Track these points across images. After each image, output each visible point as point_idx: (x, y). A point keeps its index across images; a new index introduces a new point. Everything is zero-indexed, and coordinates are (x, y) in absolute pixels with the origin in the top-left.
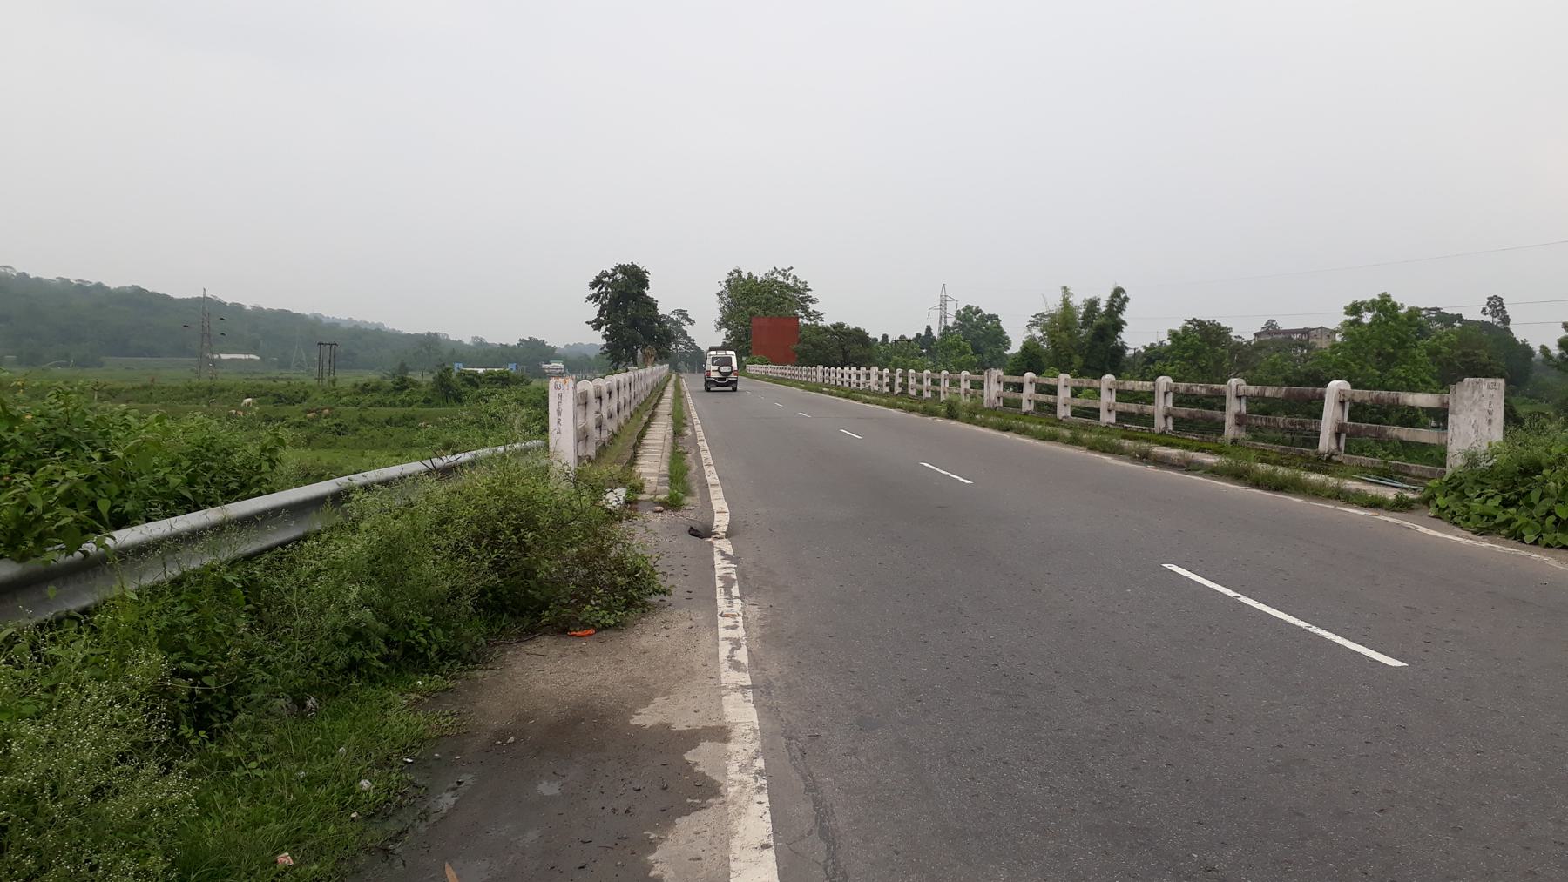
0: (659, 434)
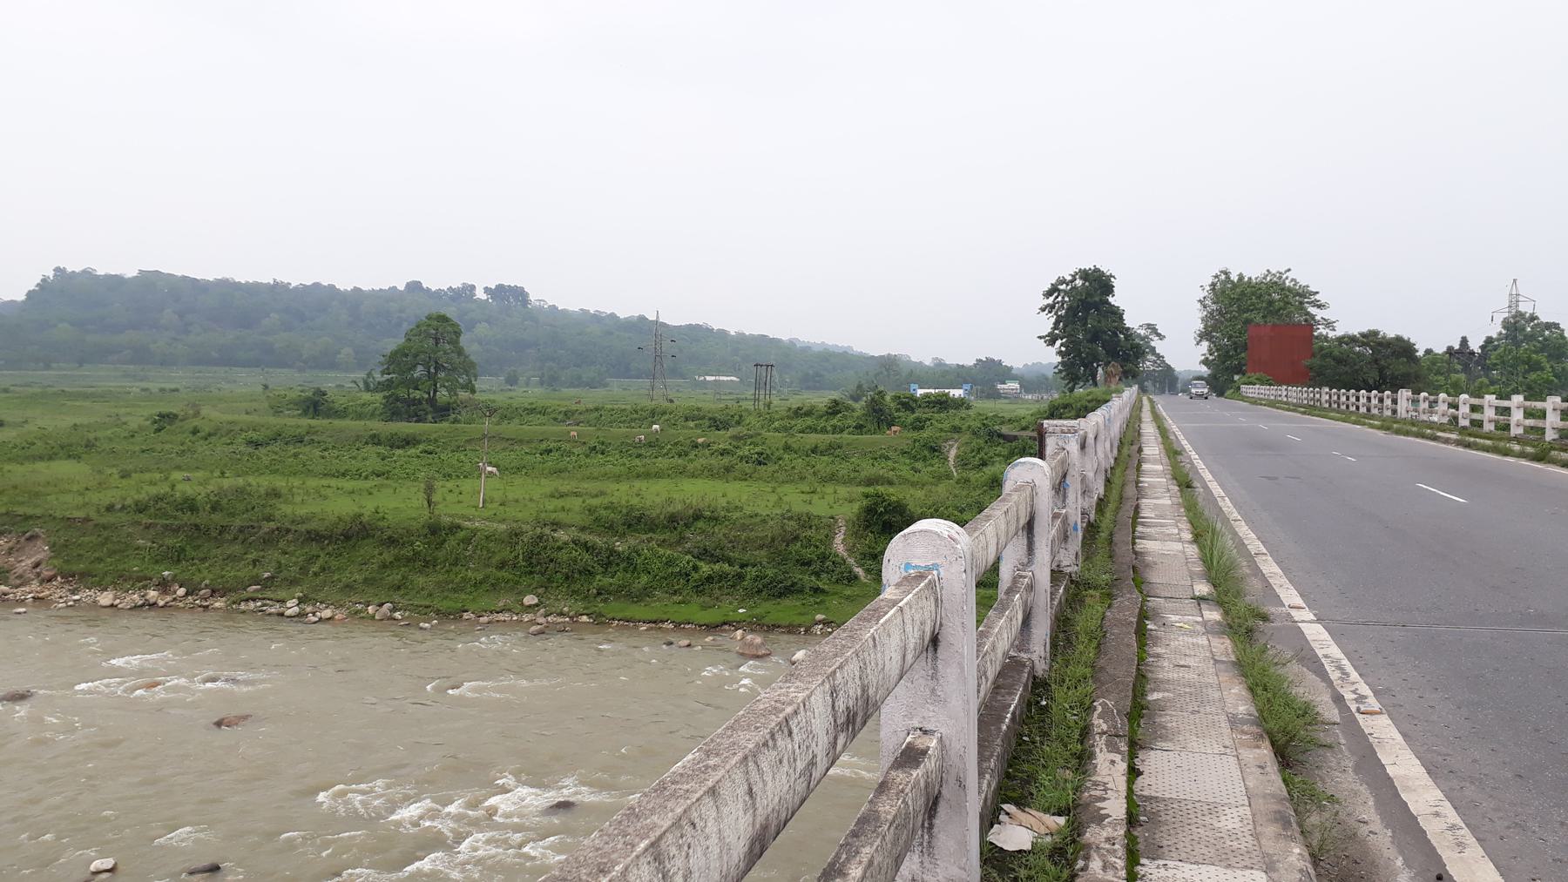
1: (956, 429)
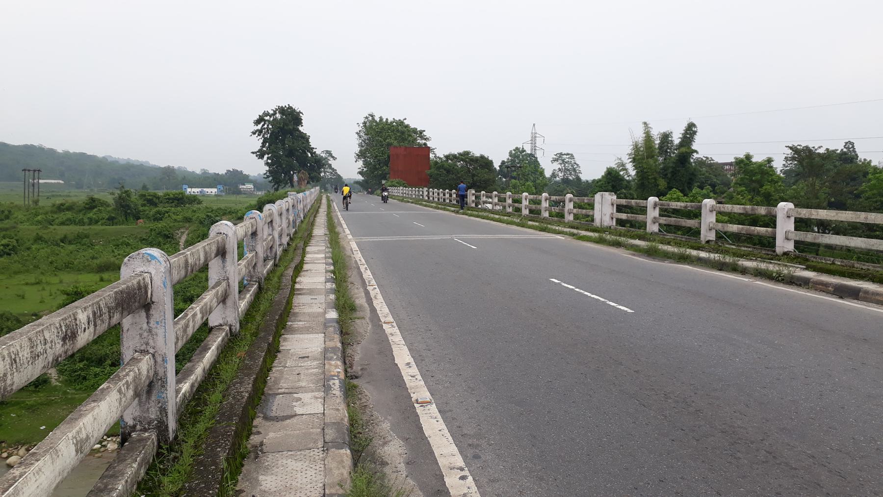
0: (317, 258)
1: (188, 220)
